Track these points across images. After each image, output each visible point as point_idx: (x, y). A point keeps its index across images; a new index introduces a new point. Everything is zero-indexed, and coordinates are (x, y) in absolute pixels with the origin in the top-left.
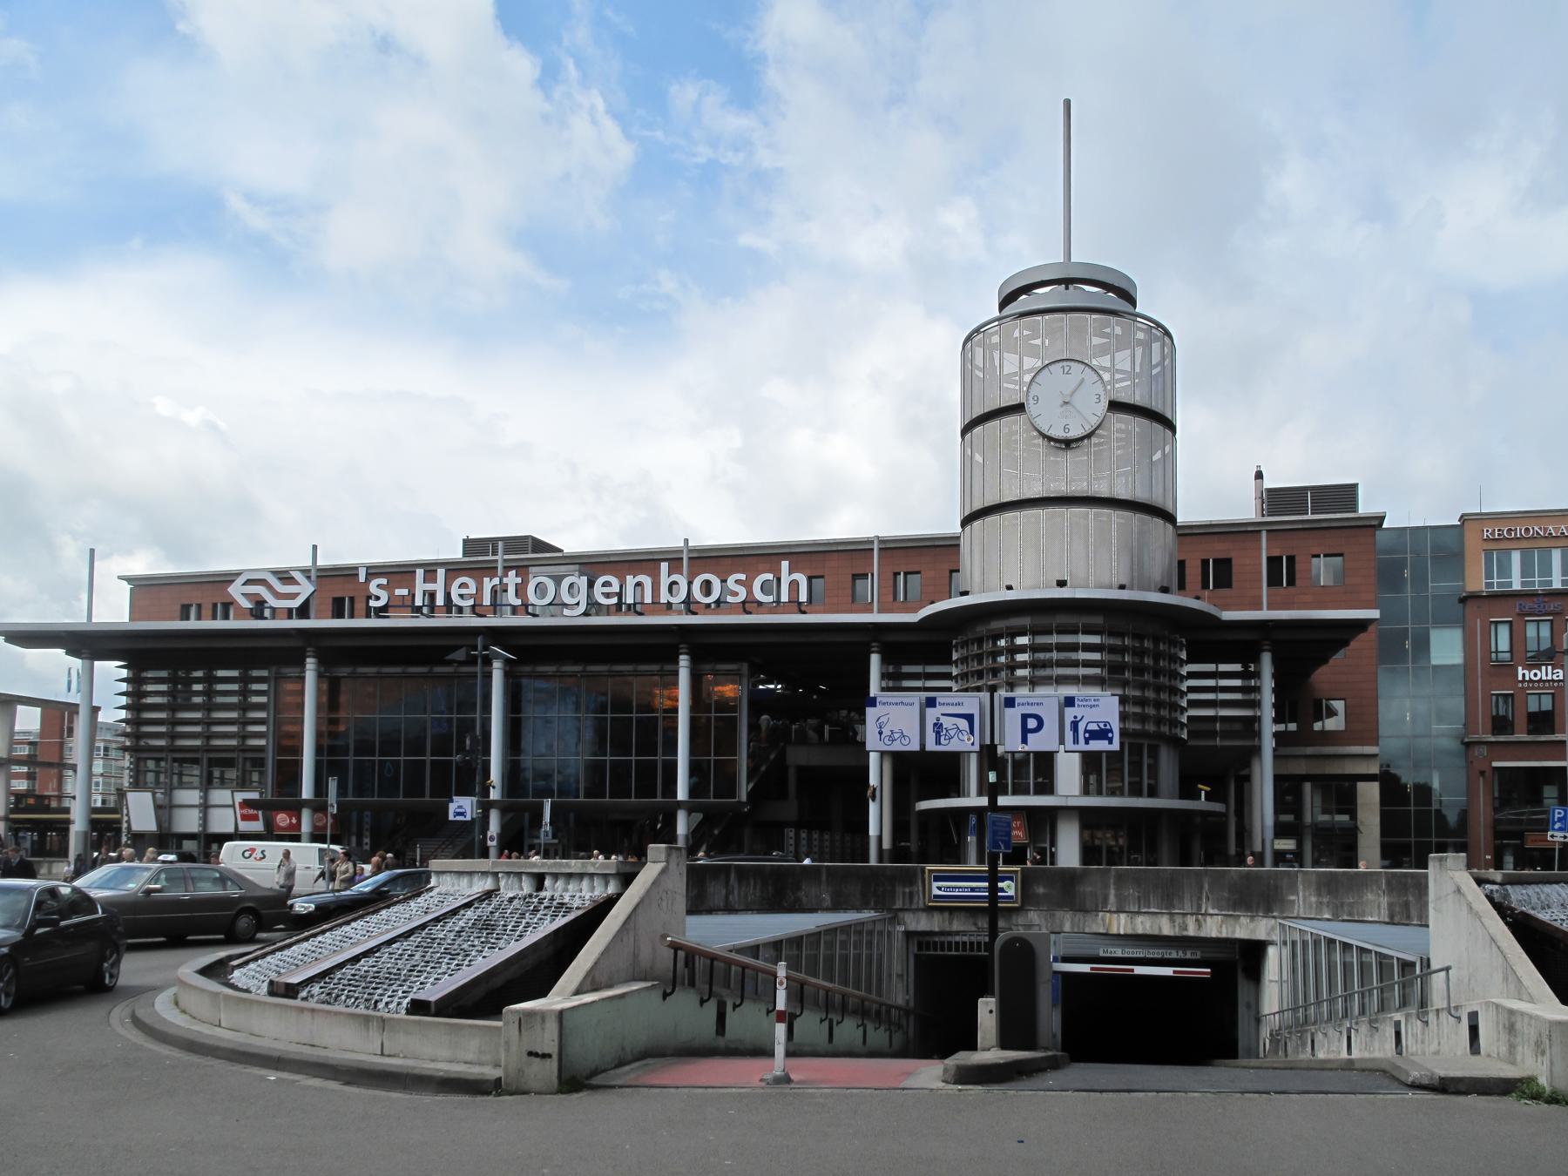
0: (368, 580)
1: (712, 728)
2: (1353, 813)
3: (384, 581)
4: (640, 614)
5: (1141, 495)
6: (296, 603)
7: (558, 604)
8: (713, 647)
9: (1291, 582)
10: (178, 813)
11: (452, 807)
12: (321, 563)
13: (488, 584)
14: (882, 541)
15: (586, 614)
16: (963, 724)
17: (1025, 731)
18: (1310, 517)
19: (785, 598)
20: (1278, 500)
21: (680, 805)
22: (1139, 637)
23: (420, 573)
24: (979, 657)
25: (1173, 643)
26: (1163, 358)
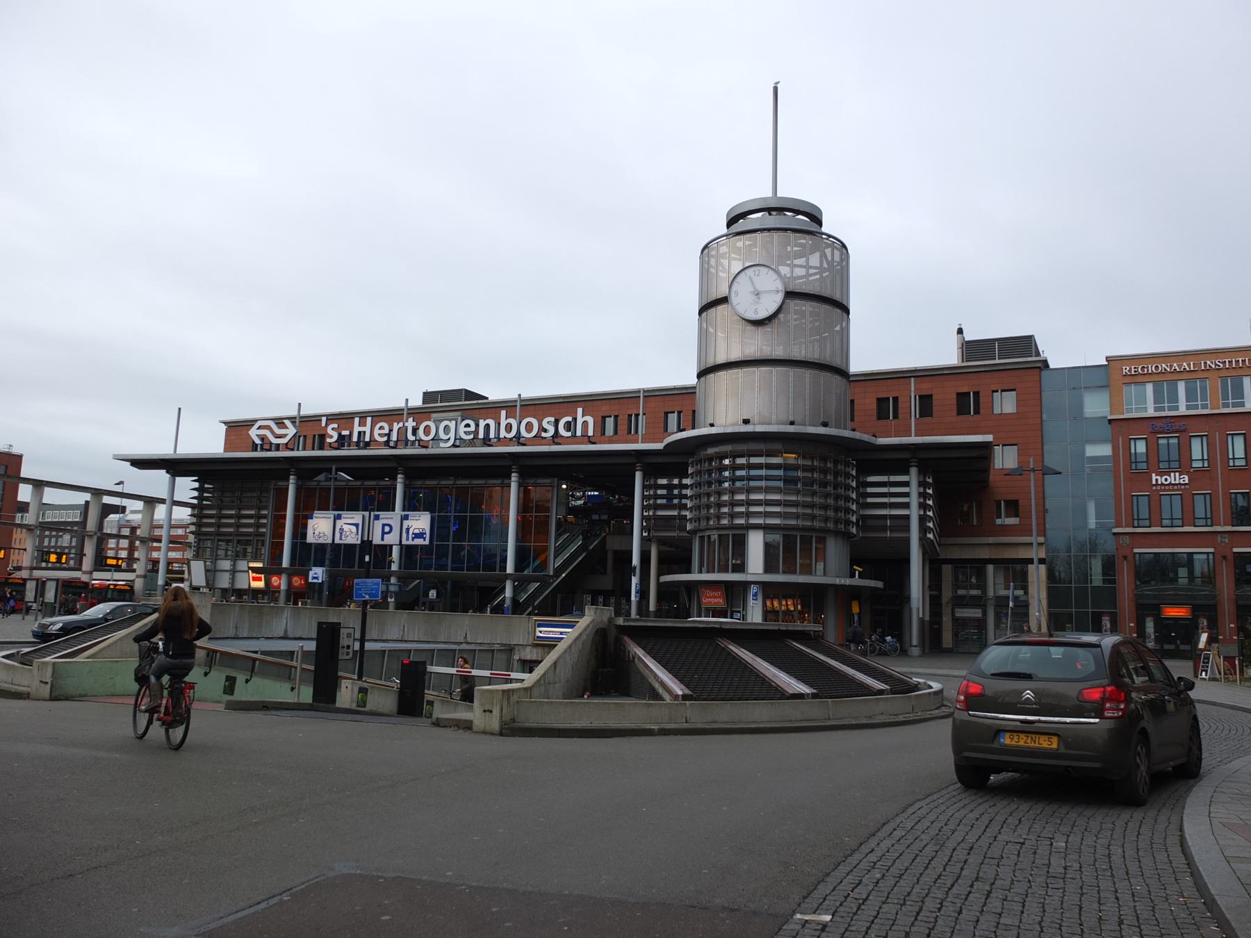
0: (327, 425)
1: (531, 525)
2: (1025, 588)
3: (335, 426)
4: (524, 445)
5: (812, 354)
6: (284, 441)
7: (436, 439)
8: (534, 467)
9: (977, 412)
10: (239, 575)
11: (311, 573)
12: (302, 413)
13: (396, 427)
14: (645, 391)
15: (454, 446)
16: (354, 529)
17: (384, 533)
18: (997, 361)
19: (579, 433)
20: (972, 349)
21: (508, 576)
22: (824, 459)
23: (357, 420)
24: (710, 472)
25: (847, 464)
26: (842, 260)
